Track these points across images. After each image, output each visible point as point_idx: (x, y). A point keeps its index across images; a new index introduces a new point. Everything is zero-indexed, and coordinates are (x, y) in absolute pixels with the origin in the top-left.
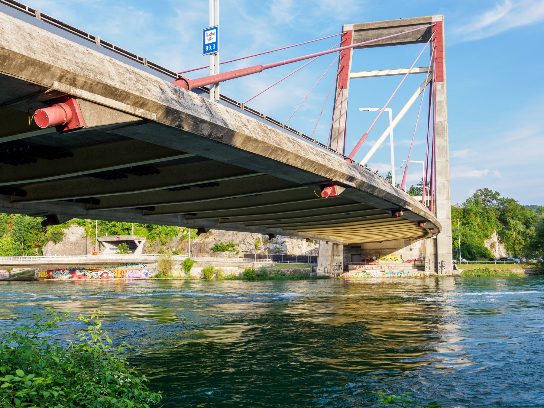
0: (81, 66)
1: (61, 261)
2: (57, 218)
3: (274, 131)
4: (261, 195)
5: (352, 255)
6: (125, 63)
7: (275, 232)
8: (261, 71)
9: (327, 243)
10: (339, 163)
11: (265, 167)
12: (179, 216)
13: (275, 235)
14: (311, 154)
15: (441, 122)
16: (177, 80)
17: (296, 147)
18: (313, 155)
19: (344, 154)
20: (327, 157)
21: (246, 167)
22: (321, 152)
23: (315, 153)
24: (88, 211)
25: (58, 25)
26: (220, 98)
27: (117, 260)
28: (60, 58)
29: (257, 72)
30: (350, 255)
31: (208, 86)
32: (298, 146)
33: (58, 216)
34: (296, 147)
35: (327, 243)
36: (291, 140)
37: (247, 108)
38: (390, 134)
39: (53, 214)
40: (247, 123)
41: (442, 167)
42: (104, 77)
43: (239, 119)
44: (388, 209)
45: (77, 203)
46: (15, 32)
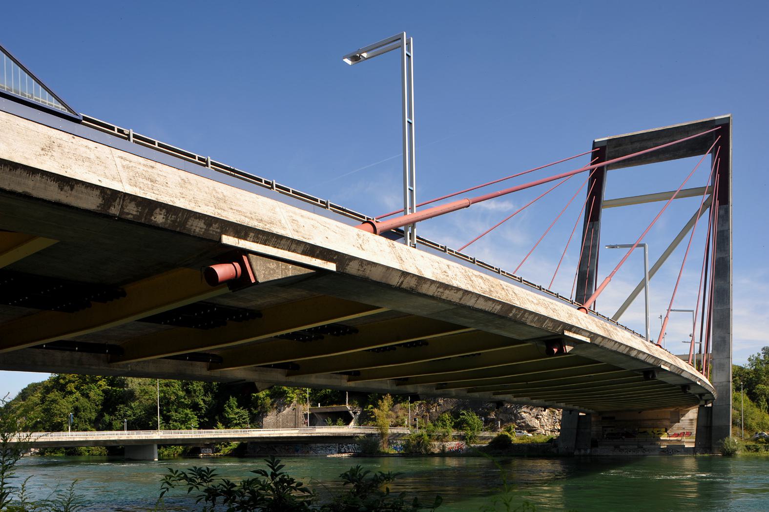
0: (250, 215)
1: (279, 434)
2: (255, 385)
3: (482, 278)
4: (480, 354)
5: (603, 427)
6: (480, 272)
7: (503, 399)
8: (468, 206)
9: (570, 413)
10: (568, 313)
11: (473, 321)
12: (388, 382)
13: (504, 403)
14: (529, 303)
15: (723, 258)
16: (364, 222)
17: (510, 296)
18: (533, 305)
19: (594, 309)
20: (551, 306)
21: (451, 321)
22: (544, 300)
23: (535, 301)
24: (287, 378)
25: (229, 172)
26: (417, 241)
27: (339, 434)
28: (226, 209)
29: (463, 208)
30: (601, 428)
31: (402, 228)
32: (513, 294)
33: (257, 384)
34: (510, 296)
35: (570, 413)
36: (505, 287)
37: (453, 251)
38: (649, 279)
39: (251, 381)
40: (448, 269)
41: (722, 317)
42: (275, 226)
43: (436, 265)
44: (638, 370)
45: (276, 369)
46: (179, 186)
